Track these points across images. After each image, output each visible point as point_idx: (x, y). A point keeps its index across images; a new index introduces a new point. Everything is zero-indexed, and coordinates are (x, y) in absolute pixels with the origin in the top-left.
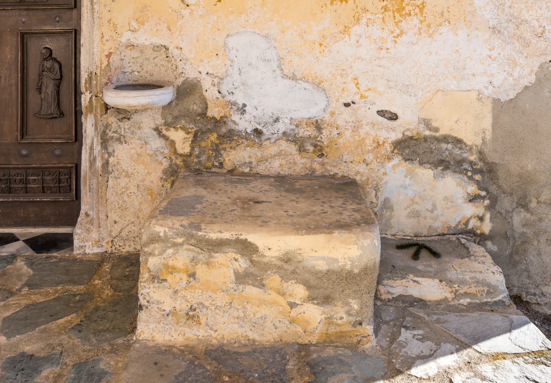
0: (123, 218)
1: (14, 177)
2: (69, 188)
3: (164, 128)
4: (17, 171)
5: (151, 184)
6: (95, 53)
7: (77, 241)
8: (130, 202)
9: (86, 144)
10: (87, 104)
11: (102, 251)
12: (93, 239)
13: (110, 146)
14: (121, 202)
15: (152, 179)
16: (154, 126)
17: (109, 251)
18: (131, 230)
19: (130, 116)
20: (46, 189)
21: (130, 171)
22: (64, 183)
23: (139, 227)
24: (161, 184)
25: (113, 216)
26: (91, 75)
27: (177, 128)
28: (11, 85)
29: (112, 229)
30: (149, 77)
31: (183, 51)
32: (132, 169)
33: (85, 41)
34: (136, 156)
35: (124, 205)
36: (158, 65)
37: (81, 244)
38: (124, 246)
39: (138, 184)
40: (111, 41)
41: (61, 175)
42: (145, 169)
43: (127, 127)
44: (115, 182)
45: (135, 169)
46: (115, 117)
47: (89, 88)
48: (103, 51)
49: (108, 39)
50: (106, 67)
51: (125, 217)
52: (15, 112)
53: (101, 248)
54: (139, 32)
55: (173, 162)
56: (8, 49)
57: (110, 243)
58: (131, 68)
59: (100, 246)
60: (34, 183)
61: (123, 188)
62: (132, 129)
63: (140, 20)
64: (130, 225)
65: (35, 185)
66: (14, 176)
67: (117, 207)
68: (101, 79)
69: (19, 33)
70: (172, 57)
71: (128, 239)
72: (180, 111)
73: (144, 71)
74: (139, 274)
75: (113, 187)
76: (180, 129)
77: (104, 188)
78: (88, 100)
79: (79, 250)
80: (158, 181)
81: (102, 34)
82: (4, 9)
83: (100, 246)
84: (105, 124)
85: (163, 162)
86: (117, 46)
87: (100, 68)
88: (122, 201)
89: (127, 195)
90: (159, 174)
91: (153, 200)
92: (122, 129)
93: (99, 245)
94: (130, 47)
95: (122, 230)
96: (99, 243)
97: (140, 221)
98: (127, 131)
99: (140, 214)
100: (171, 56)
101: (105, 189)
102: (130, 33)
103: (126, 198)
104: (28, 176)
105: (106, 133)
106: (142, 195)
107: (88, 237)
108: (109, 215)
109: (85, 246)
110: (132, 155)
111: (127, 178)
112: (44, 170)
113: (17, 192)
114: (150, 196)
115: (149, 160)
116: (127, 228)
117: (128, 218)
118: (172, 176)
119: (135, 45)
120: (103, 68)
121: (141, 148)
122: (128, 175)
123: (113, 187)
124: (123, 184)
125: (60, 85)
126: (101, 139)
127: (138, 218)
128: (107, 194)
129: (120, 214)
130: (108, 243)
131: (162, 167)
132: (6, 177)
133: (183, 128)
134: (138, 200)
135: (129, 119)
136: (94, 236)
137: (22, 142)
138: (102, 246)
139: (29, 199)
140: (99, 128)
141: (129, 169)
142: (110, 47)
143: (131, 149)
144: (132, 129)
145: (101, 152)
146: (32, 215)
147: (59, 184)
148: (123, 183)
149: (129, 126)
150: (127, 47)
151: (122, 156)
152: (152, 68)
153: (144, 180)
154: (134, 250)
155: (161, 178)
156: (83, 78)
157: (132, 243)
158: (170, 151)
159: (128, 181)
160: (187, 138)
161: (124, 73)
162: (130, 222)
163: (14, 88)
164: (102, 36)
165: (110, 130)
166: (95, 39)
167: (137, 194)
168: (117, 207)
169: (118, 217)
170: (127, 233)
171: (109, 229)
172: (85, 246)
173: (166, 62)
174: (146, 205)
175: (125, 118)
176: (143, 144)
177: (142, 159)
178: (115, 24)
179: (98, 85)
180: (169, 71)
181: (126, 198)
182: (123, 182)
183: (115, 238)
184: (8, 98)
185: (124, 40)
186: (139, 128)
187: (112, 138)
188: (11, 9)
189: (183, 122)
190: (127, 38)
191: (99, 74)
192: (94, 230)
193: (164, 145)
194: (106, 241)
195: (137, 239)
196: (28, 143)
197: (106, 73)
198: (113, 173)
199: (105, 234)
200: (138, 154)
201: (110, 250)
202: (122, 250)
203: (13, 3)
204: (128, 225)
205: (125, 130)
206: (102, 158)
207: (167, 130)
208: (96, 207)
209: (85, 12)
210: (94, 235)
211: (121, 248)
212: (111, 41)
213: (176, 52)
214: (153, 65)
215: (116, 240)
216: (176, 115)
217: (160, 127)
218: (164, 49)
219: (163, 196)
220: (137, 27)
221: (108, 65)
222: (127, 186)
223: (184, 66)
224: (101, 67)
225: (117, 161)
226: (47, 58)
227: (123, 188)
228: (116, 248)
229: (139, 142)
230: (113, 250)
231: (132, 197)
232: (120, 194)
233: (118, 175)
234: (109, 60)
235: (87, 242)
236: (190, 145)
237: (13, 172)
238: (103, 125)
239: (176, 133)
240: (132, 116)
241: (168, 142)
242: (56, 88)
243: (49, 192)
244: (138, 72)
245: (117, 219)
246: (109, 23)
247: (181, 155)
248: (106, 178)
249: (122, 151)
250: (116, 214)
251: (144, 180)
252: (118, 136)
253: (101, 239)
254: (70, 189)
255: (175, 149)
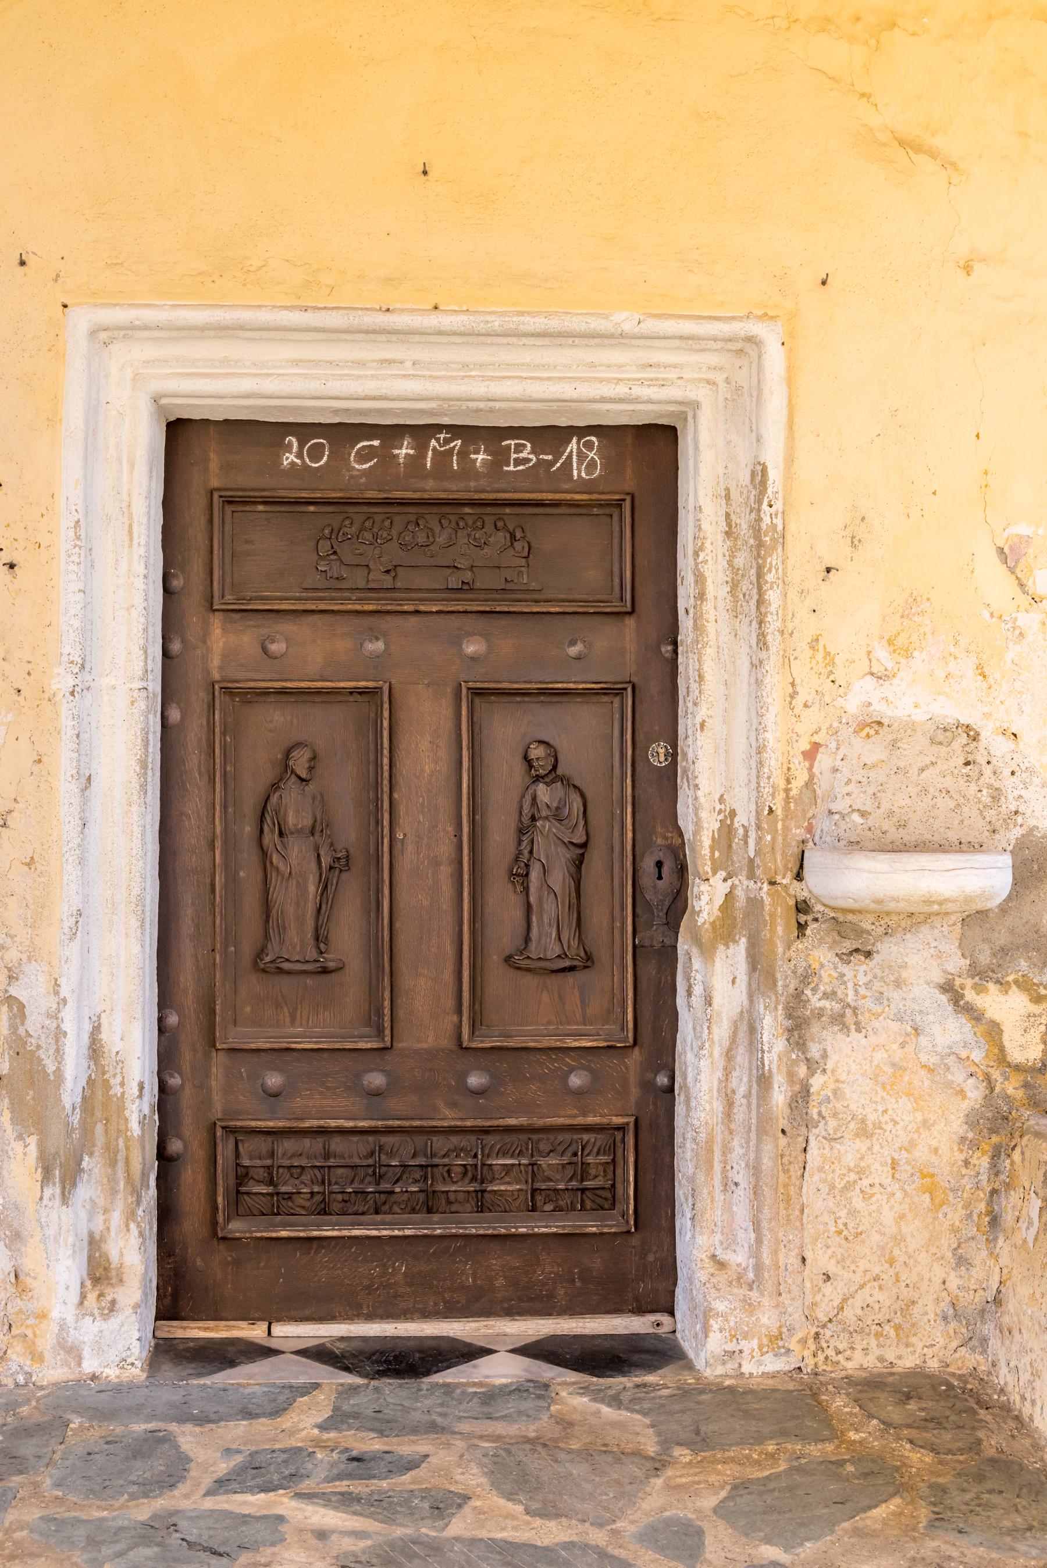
0: (848, 1263)
1: (446, 1161)
2: (609, 1195)
3: (969, 982)
4: (455, 1140)
5: (934, 1158)
6: (770, 745)
7: (718, 1335)
8: (870, 1214)
9: (713, 1042)
10: (716, 913)
11: (787, 1368)
12: (764, 1330)
13: (813, 1040)
14: (843, 1214)
15: (934, 1143)
16: (938, 978)
17: (807, 1366)
18: (870, 1300)
19: (873, 944)
20: (539, 1198)
21: (872, 1117)
22: (596, 1177)
23: (895, 1290)
24: (960, 1157)
25: (821, 1260)
26: (732, 820)
27: (1008, 983)
28: (436, 863)
29: (818, 1298)
30: (894, 829)
31: (1021, 744)
32: (876, 1110)
33: (710, 713)
34: (889, 1070)
35: (851, 1225)
36: (932, 790)
37: (729, 1347)
38: (848, 1353)
39: (893, 1159)
40: (817, 706)
41: (586, 1152)
42: (915, 1110)
43: (862, 980)
44: (827, 1151)
45: (885, 1111)
46: (830, 948)
47: (724, 863)
48: (795, 737)
49: (810, 700)
50: (804, 790)
51: (853, 1262)
52: (449, 949)
53: (784, 1358)
54: (895, 681)
55: (997, 1090)
56: (425, 744)
57: (811, 1341)
58: (848, 801)
59: (783, 1350)
60: (507, 1179)
61: (850, 1170)
62: (877, 985)
63: (900, 641)
64: (869, 1285)
65: (509, 1183)
66: (444, 1156)
67: (833, 1229)
68: (786, 829)
69: (464, 691)
70: (984, 763)
71: (862, 1331)
72: (1012, 931)
73: (882, 810)
74: (536, 1547)
75: (821, 1169)
76: (1014, 987)
77: (795, 1170)
78: (719, 900)
79: (724, 1363)
80: (952, 1149)
81: (793, 684)
82: (417, 612)
83: (783, 1350)
84: (800, 971)
85: (966, 1089)
86: (836, 724)
87: (782, 795)
88: (846, 1211)
89: (862, 1192)
90: (957, 1126)
91: (936, 1206)
92: (850, 985)
93: (779, 1348)
94: (867, 730)
95: (845, 1300)
96: (781, 1343)
97: (897, 1274)
98: (862, 991)
99: (896, 1252)
100: (982, 760)
101: (799, 1173)
102: (870, 682)
103: (858, 1203)
104: (488, 1156)
105: (804, 998)
106: (905, 1191)
107: (747, 1325)
108: (808, 1255)
109: (741, 1351)
110: (877, 1066)
111: (863, 1138)
112: (535, 1137)
113: (454, 1208)
114: (927, 1196)
115: (927, 1083)
116: (859, 1296)
117: (863, 1264)
118: (993, 1131)
119: (886, 721)
120: (794, 792)
121: (902, 1046)
122: (864, 1131)
123: (821, 1169)
124: (850, 1159)
125: (581, 862)
126: (789, 1016)
127: (892, 1262)
128: (804, 1190)
129: (840, 1252)
130: (803, 1341)
131: (965, 1106)
132: (421, 1161)
133: (1025, 985)
134: (892, 1208)
135: (868, 954)
136: (765, 1320)
137: (474, 1045)
138: (788, 1350)
139: (494, 1228)
140: (780, 983)
141: (868, 1110)
142: (814, 727)
143: (875, 1048)
144: (877, 985)
145: (789, 1059)
146: (500, 1282)
147: (582, 1180)
148: (850, 1156)
149: (869, 977)
150: (863, 726)
151: (849, 1072)
152: (908, 801)
153: (912, 1144)
154: (879, 1365)
155: (963, 1139)
156: (705, 832)
157: (873, 1343)
158: (987, 1056)
159: (863, 1150)
160: (1035, 1016)
161: (831, 813)
162: (868, 1276)
163: (445, 871)
164: (791, 690)
165: (814, 990)
166: (770, 700)
167: (889, 1189)
168: (833, 1229)
169: (833, 1261)
170: (859, 1312)
171: (809, 1300)
172: (741, 1351)
173: (962, 781)
174: (916, 1222)
175: (857, 950)
176: (907, 1035)
177: (907, 1078)
178: (829, 653)
179: (779, 846)
180: (965, 809)
181: (858, 1203)
182: (850, 1151)
183: (824, 1326)
184: (425, 903)
185: (852, 705)
186: (898, 984)
187: (820, 1014)
188: (437, 612)
189: (1024, 964)
190: (864, 699)
191: (779, 812)
192: (766, 1301)
193: (969, 1037)
194: (800, 1335)
195: (887, 1327)
196: (492, 1048)
197: (804, 810)
198: (821, 1125)
199: (796, 1317)
200: (893, 1065)
201: (810, 1362)
202: (843, 1362)
203: (435, 590)
204: (862, 1287)
205: (856, 991)
206: (791, 1076)
207: (979, 989)
208: (771, 1230)
209: (711, 617)
210: (767, 1319)
211: (840, 1357)
212: (817, 706)
213: (1001, 747)
214: (913, 790)
215: (828, 1333)
216: (1002, 942)
217: (958, 982)
218: (964, 739)
219: (965, 1195)
220: (890, 665)
221: (809, 784)
222: (862, 1164)
223: (1023, 792)
224: (787, 791)
225: (832, 1086)
226: (547, 775)
227: (850, 1170)
228: (827, 1358)
229: (895, 1026)
230: (820, 1363)
231: (874, 1199)
232: (841, 1191)
233: (835, 1131)
234: (811, 767)
235: (745, 1338)
236: (1042, 1038)
237: (439, 1143)
238: (794, 972)
239: (1002, 998)
240: (879, 944)
241: (980, 1029)
242: (573, 869)
243: (549, 1207)
244: (863, 814)
245: (832, 1268)
246: (812, 648)
247: (1018, 1068)
248: (801, 1139)
249: (847, 1056)
250: (830, 1252)
251: (912, 1144)
252: (837, 1007)
253: (784, 1330)
254: (614, 1197)
255: (1002, 1049)
